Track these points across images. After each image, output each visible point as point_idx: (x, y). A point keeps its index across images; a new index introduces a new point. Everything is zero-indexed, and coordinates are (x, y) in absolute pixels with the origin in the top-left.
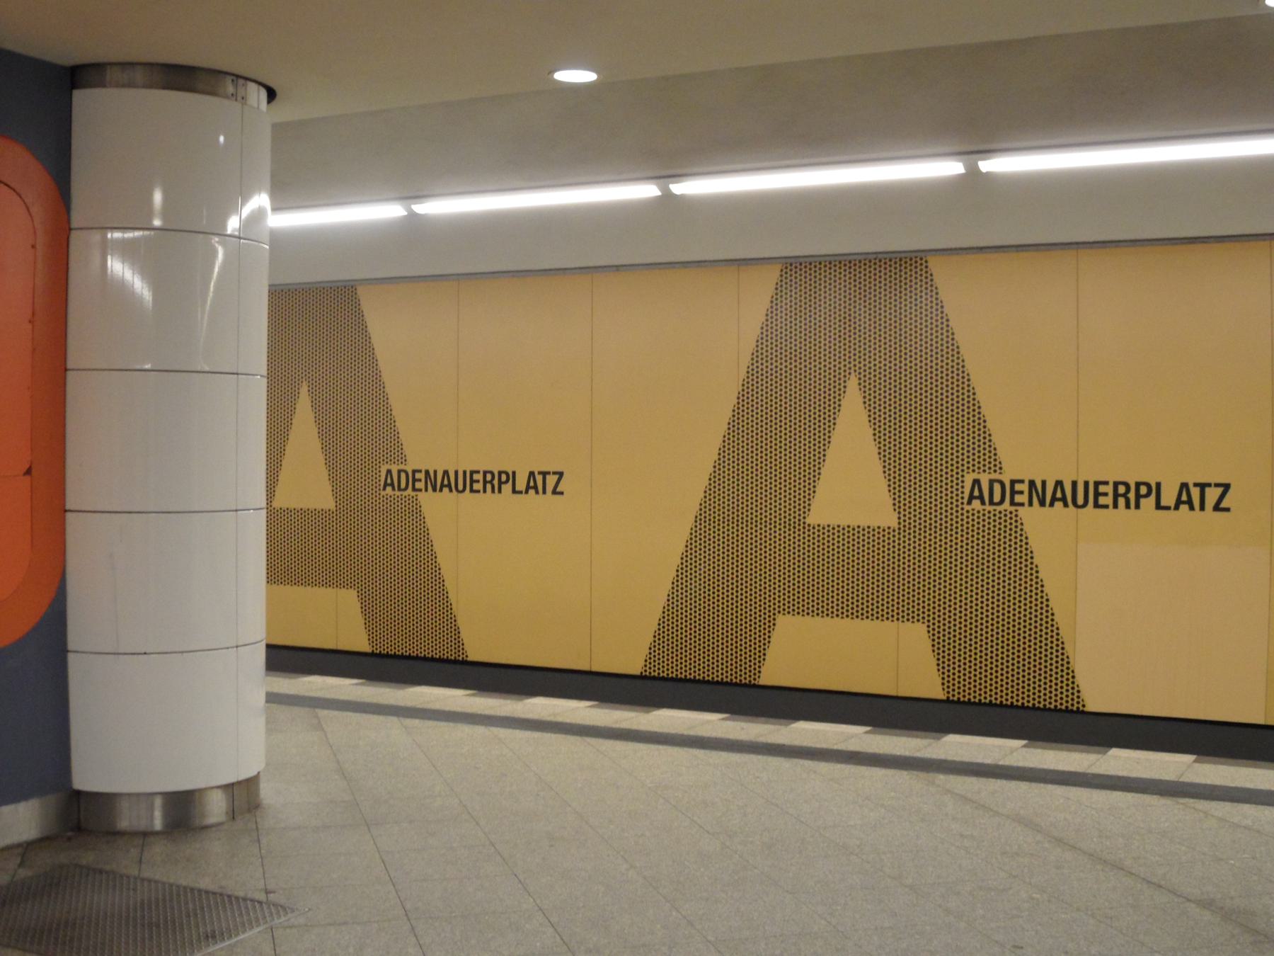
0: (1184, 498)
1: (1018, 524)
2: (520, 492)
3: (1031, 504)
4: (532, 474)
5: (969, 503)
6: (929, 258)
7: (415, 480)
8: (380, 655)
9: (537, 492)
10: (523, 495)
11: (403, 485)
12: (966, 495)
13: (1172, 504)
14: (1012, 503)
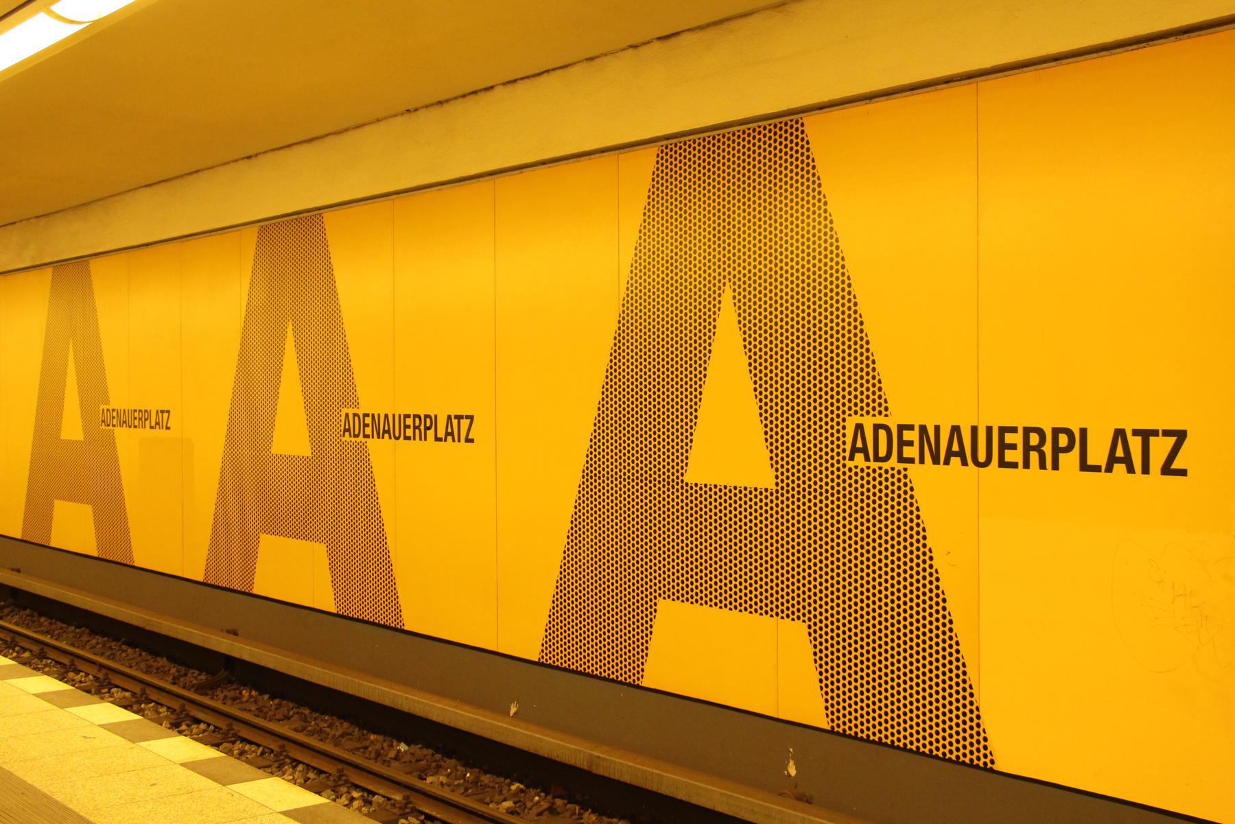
0: (1120, 453)
1: (365, 459)
2: (1097, 469)
3: (922, 461)
4: (1119, 434)
5: (852, 458)
6: (805, 121)
7: (902, 443)
8: (342, 617)
9: (1131, 470)
10: (1103, 475)
11: (882, 452)
12: (848, 447)
13: (1102, 461)
14: (901, 459)
